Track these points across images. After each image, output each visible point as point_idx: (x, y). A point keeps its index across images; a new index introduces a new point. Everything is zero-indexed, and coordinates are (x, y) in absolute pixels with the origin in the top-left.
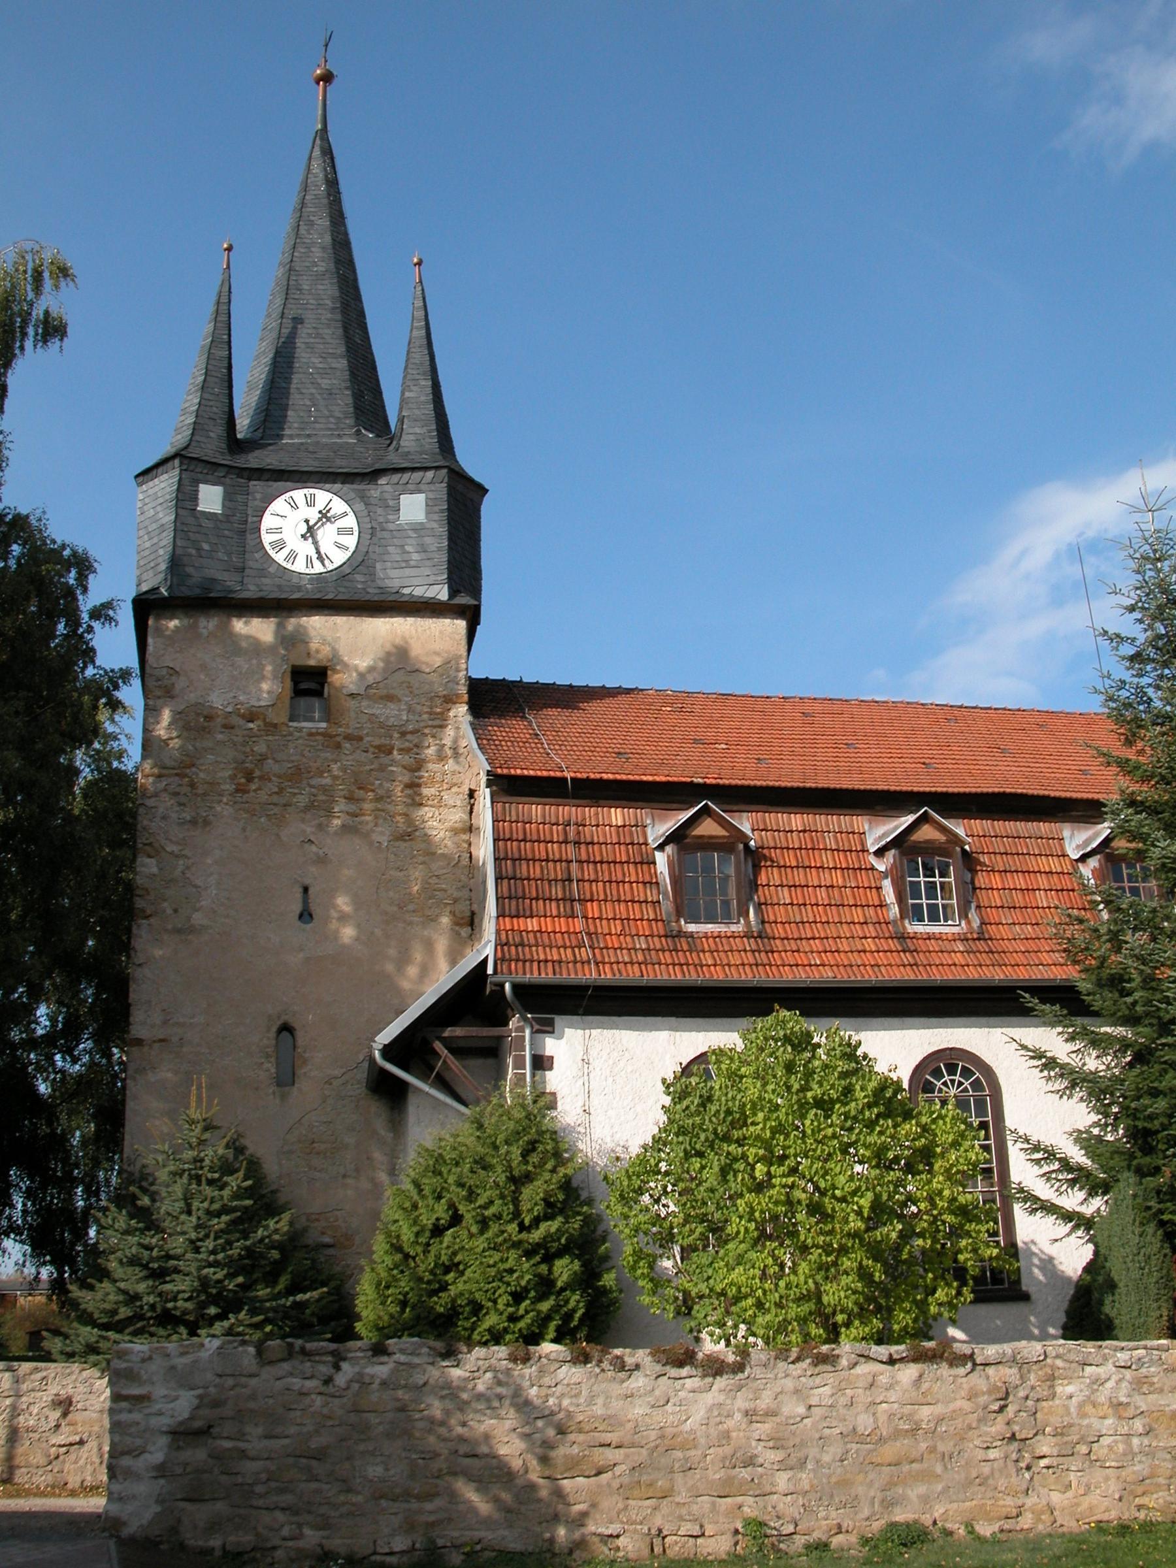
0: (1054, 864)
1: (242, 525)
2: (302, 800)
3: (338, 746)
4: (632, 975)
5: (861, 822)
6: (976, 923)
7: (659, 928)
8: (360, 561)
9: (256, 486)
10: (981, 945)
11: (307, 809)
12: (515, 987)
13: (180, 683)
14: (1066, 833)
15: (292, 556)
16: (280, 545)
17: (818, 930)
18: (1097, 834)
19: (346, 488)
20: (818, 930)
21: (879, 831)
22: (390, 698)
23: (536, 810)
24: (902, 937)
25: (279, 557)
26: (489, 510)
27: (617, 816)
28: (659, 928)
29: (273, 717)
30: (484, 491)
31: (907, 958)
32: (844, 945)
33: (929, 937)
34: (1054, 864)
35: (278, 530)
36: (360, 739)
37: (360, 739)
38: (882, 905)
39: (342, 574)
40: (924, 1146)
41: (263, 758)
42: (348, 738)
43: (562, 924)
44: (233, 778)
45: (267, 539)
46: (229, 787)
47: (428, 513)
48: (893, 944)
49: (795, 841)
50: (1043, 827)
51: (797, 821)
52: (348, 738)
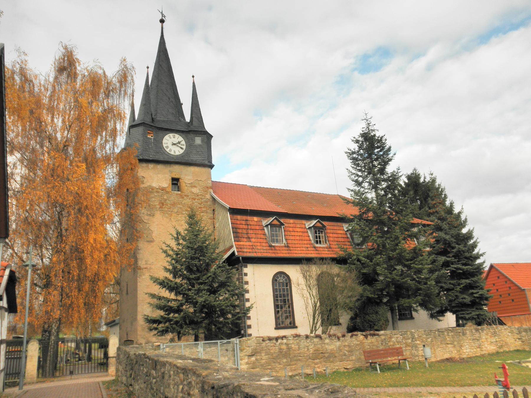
0: (341, 232)
1: (159, 143)
2: (176, 210)
3: (183, 198)
4: (259, 255)
5: (304, 222)
6: (328, 244)
7: (267, 244)
8: (186, 153)
9: (160, 133)
10: (330, 249)
11: (176, 212)
12: (242, 258)
13: (145, 180)
14: (344, 225)
15: (171, 150)
16: (167, 147)
17: (298, 245)
18: (311, 223)
19: (182, 134)
20: (298, 245)
21: (265, 222)
22: (195, 187)
23: (239, 217)
24: (315, 247)
25: (168, 150)
26: (213, 141)
27: (255, 219)
28: (267, 244)
29: (167, 190)
30: (212, 137)
31: (317, 252)
32: (304, 249)
33: (320, 247)
34: (341, 232)
35: (167, 143)
36: (188, 196)
37: (188, 196)
38: (310, 240)
39: (182, 156)
40: (420, 268)
41: (166, 200)
42: (185, 196)
43: (247, 243)
44: (159, 204)
45: (164, 145)
46: (158, 207)
47: (202, 142)
48: (314, 249)
49: (292, 225)
50: (339, 224)
51: (292, 221)
52: (185, 196)
